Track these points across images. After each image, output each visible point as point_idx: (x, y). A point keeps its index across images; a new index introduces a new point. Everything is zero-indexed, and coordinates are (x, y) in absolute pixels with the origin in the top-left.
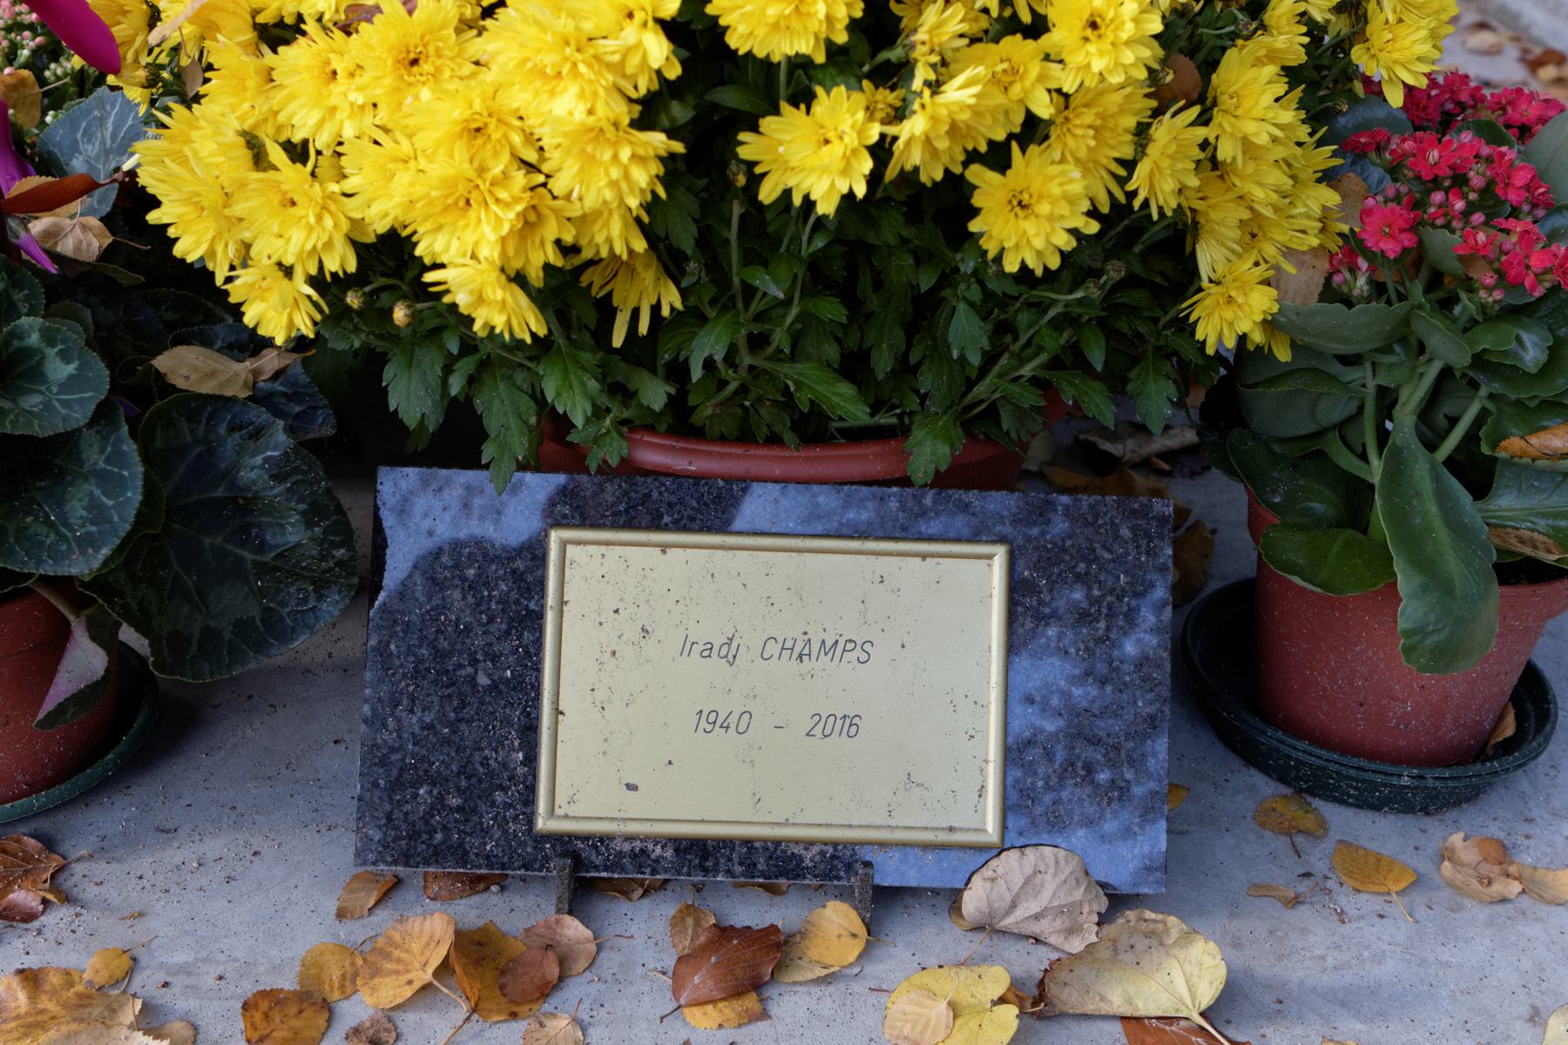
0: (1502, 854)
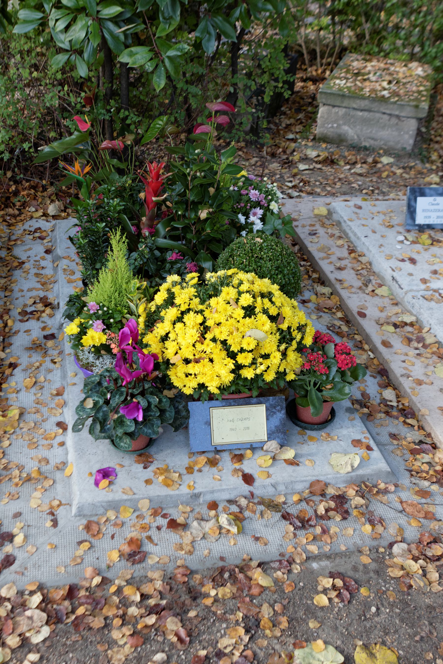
0: (329, 435)
